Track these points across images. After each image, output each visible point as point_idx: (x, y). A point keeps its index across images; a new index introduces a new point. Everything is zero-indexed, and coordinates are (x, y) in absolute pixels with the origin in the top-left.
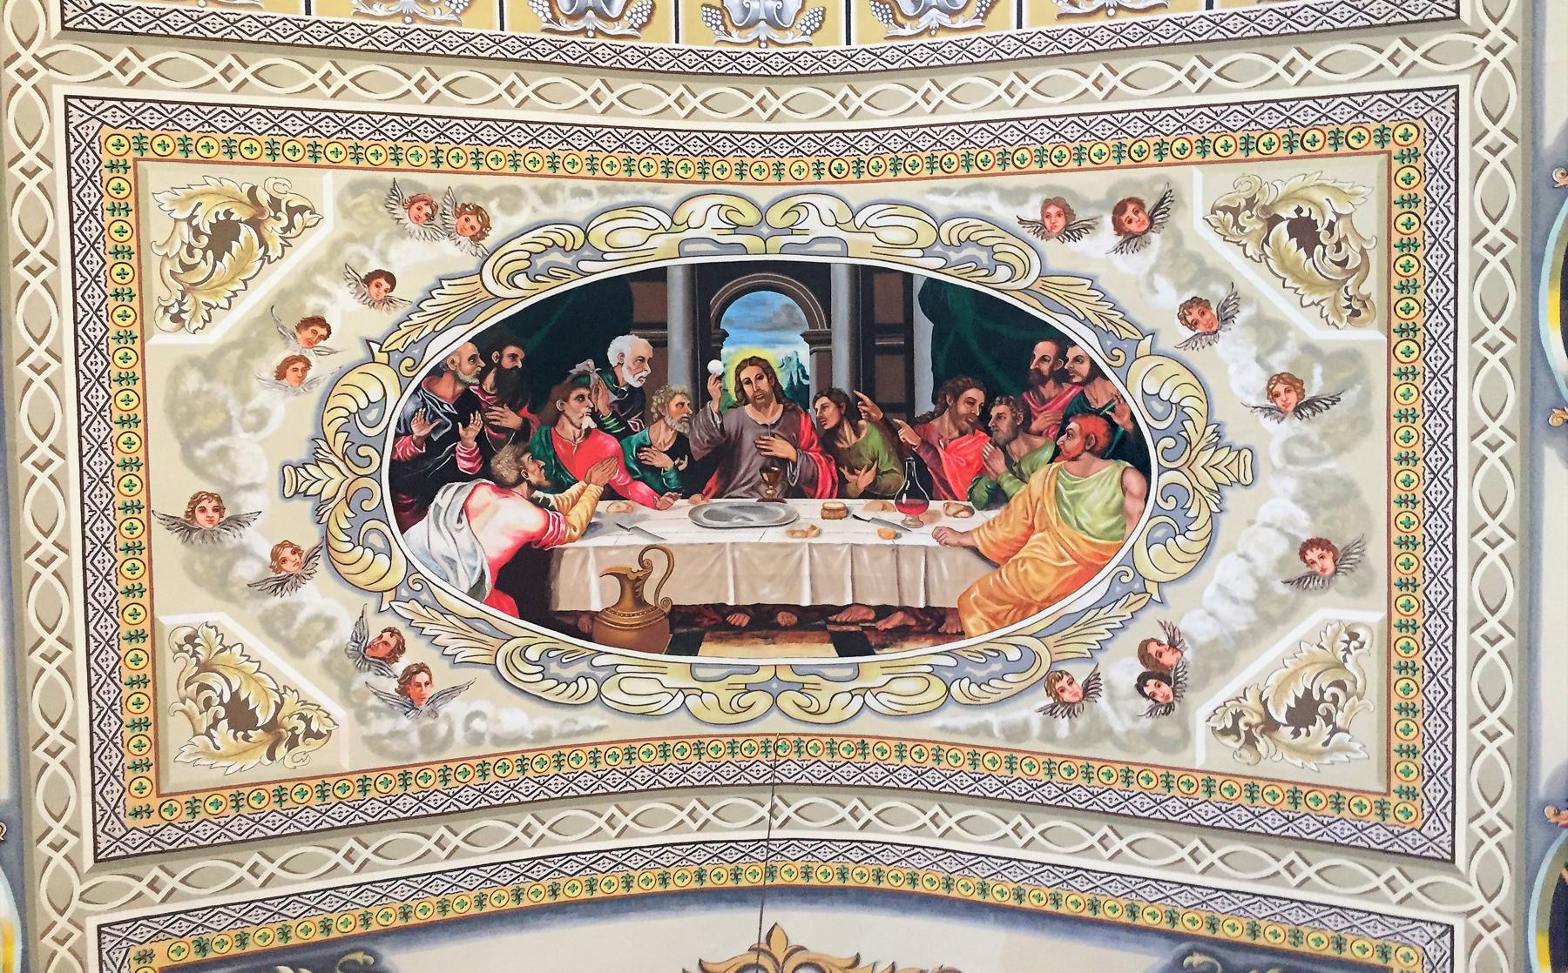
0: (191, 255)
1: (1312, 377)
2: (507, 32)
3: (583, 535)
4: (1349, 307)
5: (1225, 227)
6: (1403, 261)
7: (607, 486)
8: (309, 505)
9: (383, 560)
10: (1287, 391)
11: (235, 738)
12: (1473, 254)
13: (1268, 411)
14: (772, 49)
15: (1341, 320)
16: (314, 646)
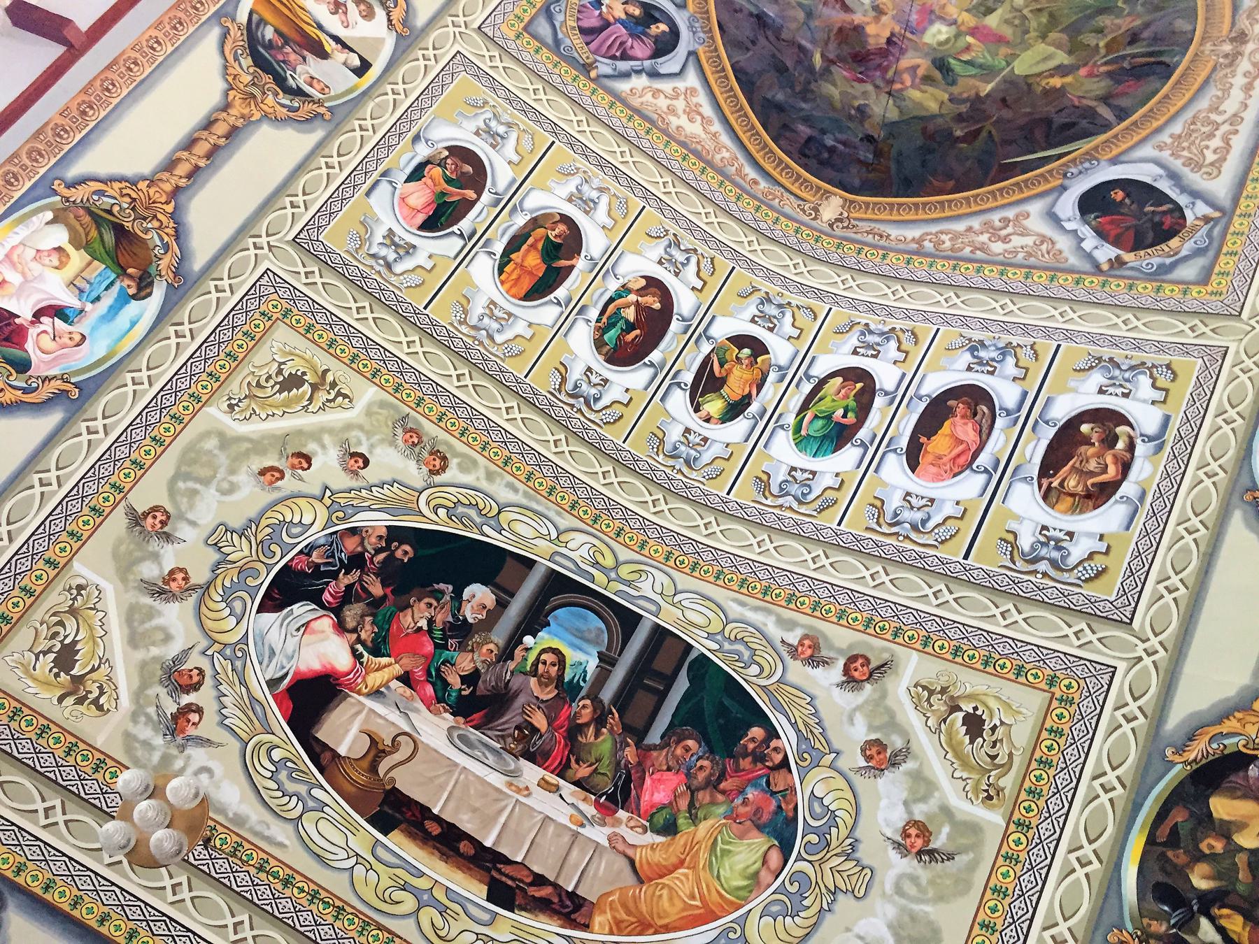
0: (267, 381)
1: (940, 833)
2: (527, 380)
3: (368, 695)
4: (986, 791)
5: (920, 701)
6: (1037, 773)
7: (407, 673)
8: (216, 556)
9: (233, 620)
10: (917, 836)
11: (51, 671)
12: (1090, 787)
13: (898, 846)
14: (679, 476)
15: (977, 797)
16: (147, 647)
